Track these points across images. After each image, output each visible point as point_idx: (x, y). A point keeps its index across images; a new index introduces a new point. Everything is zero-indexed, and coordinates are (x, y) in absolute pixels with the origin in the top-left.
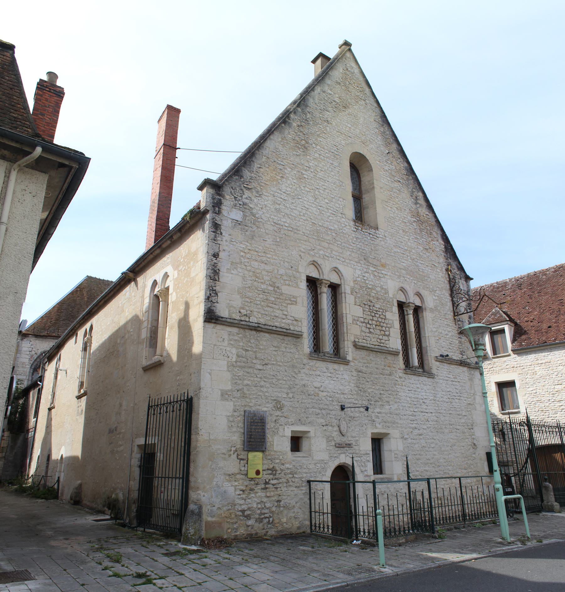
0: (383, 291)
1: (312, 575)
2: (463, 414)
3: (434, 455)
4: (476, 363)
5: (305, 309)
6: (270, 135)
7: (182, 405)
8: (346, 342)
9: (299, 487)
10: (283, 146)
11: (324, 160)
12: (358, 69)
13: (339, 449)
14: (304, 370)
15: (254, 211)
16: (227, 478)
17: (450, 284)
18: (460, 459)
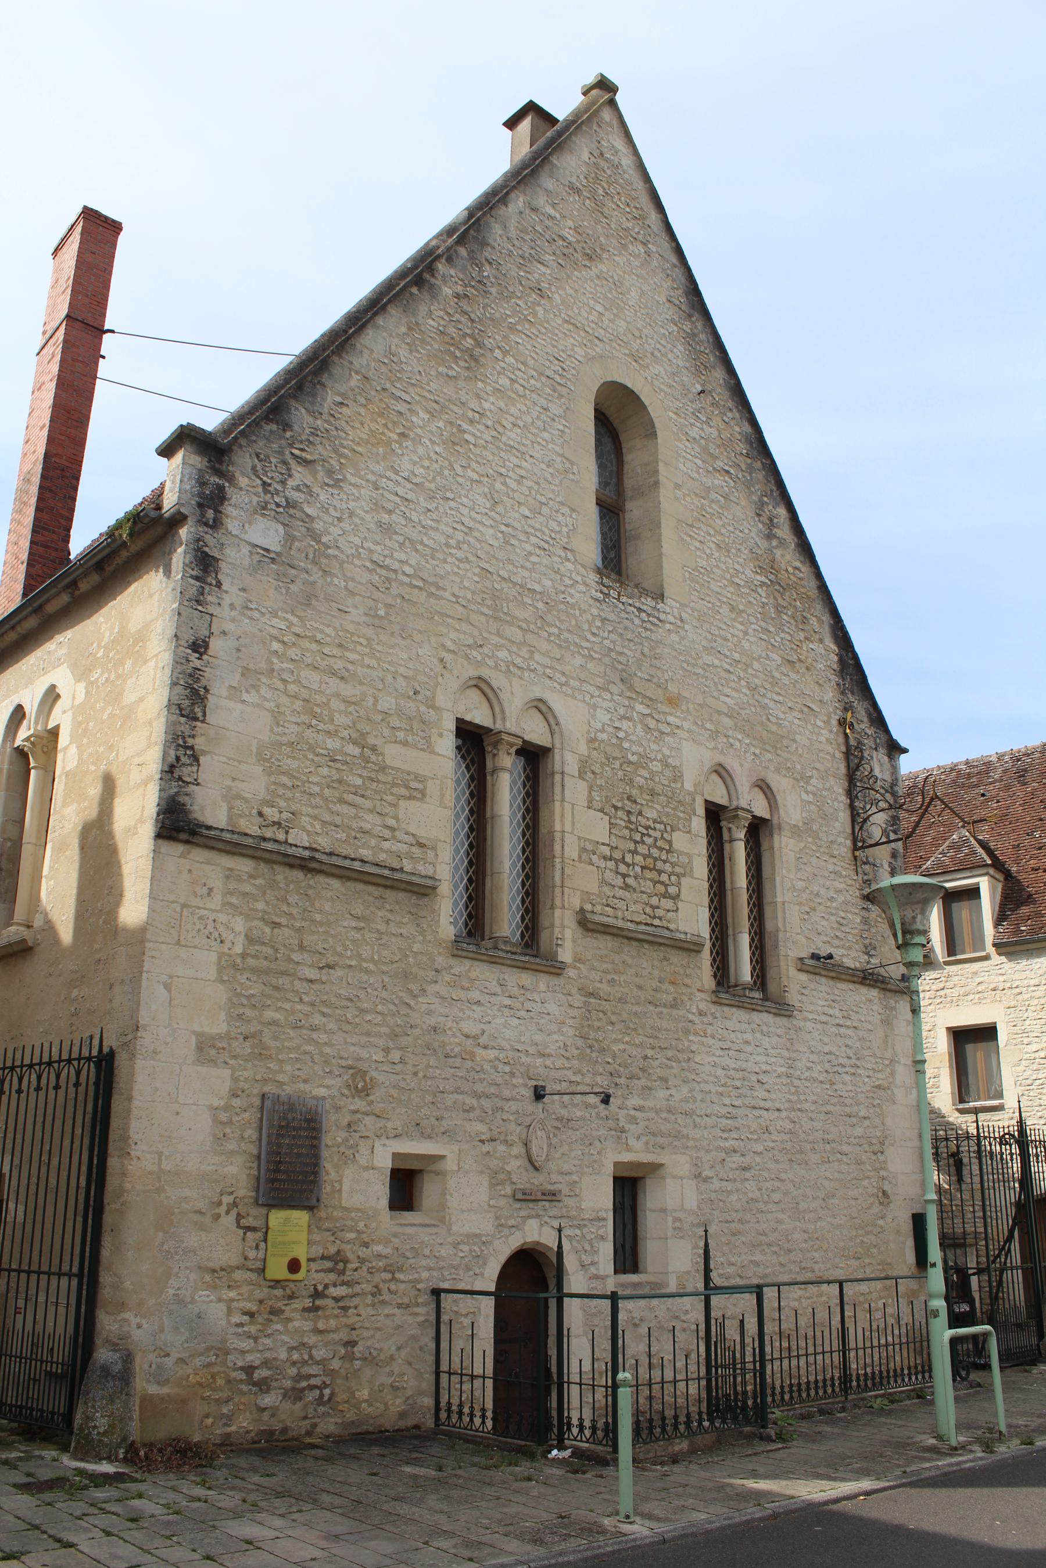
0: (668, 773)
1: (436, 1544)
2: (862, 1114)
3: (779, 1221)
4: (904, 978)
5: (449, 814)
6: (375, 314)
7: (84, 1072)
8: (558, 912)
9: (408, 1306)
10: (412, 347)
11: (524, 396)
12: (632, 158)
13: (524, 1205)
14: (435, 988)
15: (318, 526)
16: (208, 1278)
17: (848, 761)
18: (845, 1232)
